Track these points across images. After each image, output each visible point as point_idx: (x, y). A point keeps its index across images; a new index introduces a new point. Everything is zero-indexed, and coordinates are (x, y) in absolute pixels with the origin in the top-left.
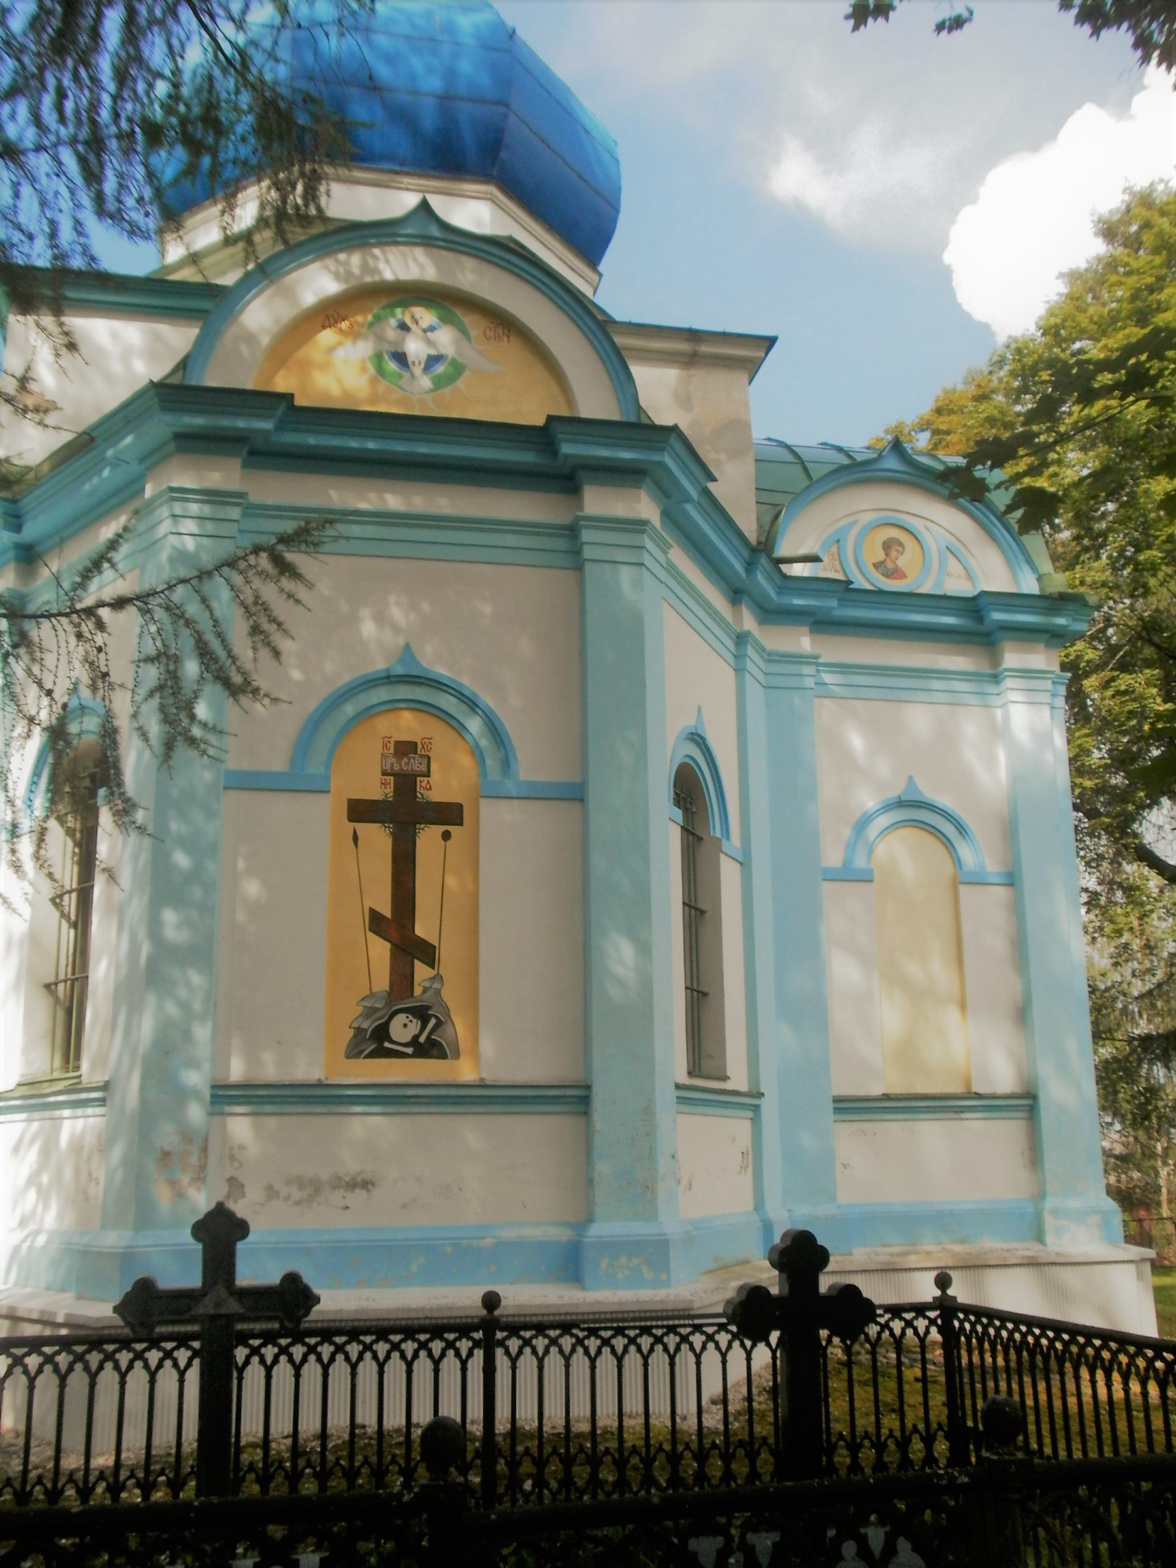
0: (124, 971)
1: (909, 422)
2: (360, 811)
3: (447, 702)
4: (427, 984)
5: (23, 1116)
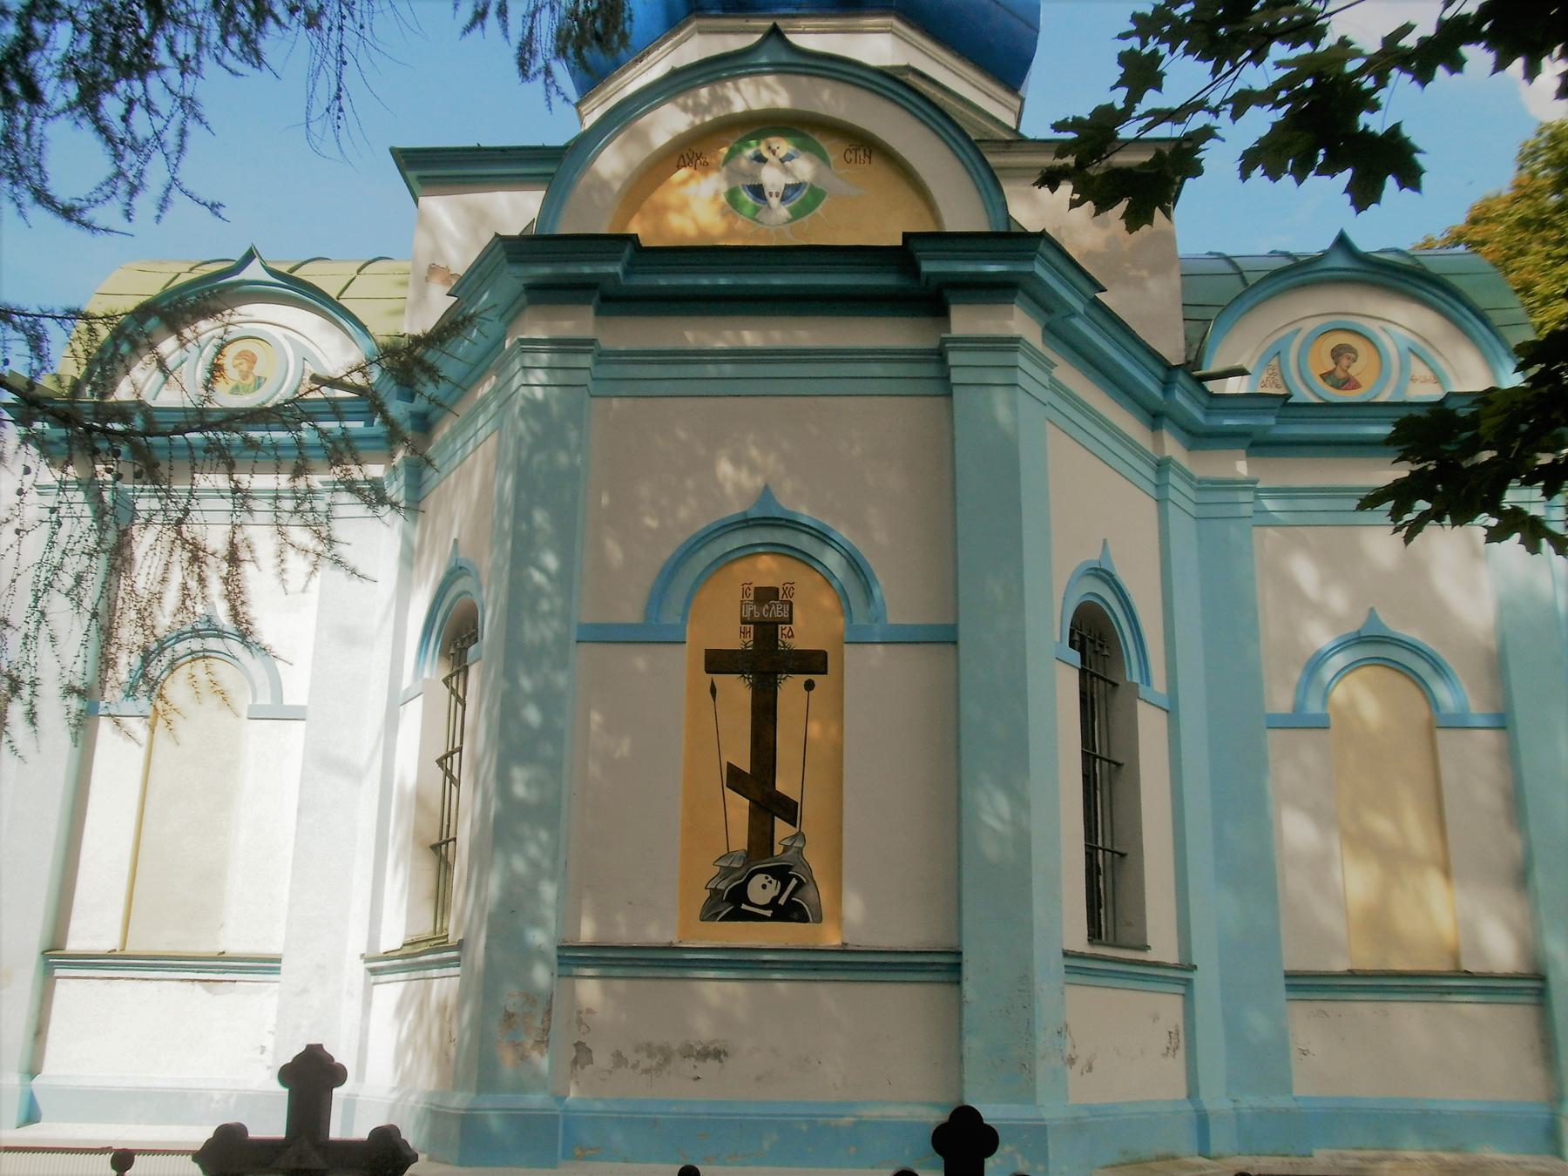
0: (477, 827)
1: (1437, 237)
2: (717, 662)
3: (804, 542)
4: (787, 842)
5: (403, 976)
